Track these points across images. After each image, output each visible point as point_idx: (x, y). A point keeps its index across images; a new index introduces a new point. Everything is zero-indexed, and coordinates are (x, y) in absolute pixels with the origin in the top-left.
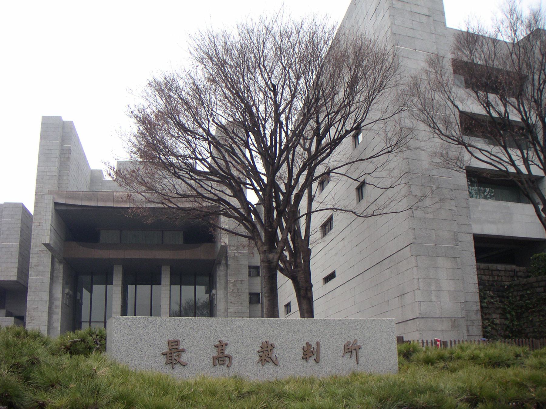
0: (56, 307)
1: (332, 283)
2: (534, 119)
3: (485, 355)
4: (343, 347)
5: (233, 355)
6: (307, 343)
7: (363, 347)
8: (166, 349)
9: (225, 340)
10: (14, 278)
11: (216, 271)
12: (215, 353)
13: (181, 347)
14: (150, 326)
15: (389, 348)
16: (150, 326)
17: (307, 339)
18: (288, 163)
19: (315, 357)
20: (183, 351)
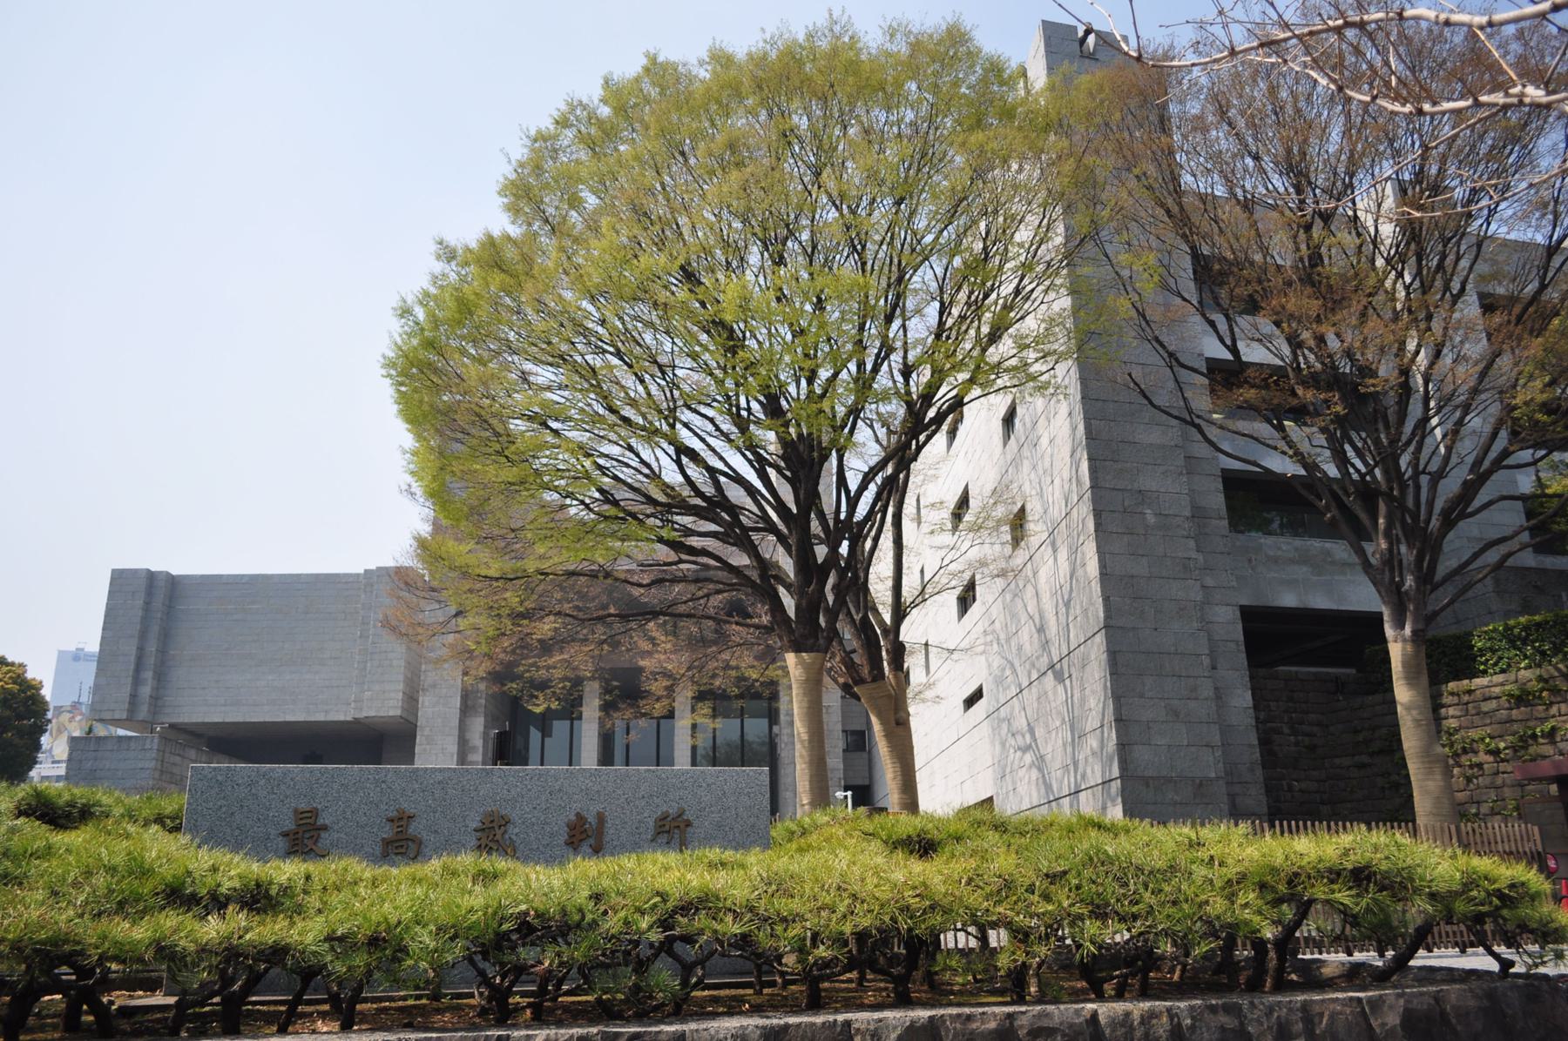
0: (474, 748)
1: (980, 707)
2: (1285, 95)
3: (447, 907)
4: (652, 824)
5: (424, 835)
6: (578, 815)
7: (695, 823)
8: (289, 825)
9: (409, 807)
10: (398, 712)
11: (106, 658)
12: (388, 832)
13: (320, 822)
14: (262, 782)
15: (753, 826)
16: (262, 782)
17: (576, 807)
18: (848, 492)
19: (592, 841)
20: (325, 828)
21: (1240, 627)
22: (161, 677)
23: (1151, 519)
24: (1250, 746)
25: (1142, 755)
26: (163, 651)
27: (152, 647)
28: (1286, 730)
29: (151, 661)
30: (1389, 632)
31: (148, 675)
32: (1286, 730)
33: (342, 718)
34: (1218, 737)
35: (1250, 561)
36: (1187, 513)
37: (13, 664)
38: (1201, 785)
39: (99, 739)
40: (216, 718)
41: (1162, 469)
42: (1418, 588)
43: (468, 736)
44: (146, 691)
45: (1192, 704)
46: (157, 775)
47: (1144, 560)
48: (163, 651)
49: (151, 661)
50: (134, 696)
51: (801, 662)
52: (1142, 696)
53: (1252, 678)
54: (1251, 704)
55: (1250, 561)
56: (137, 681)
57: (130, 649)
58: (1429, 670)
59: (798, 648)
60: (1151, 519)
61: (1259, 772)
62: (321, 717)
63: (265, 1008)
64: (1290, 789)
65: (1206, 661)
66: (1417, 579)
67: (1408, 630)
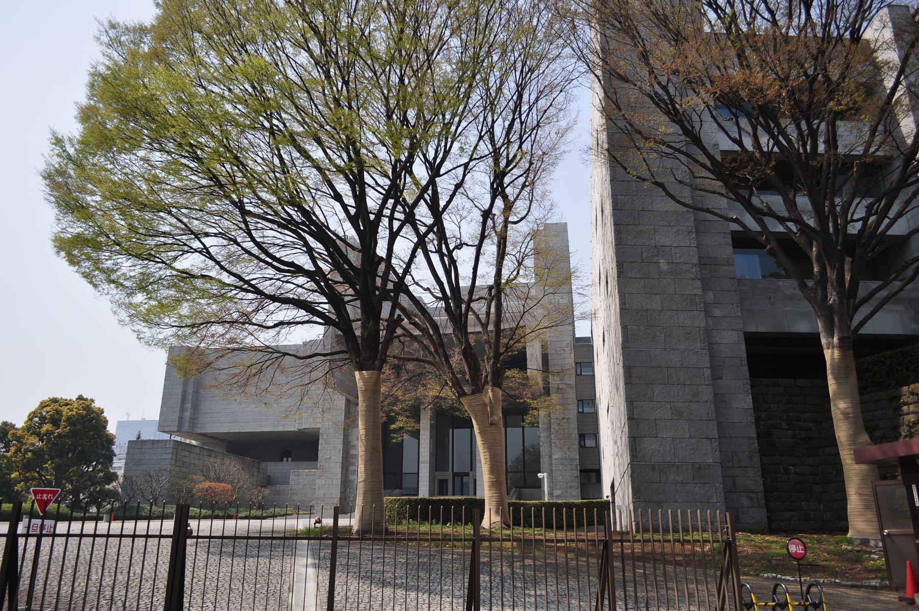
21: (743, 347)
22: (196, 407)
23: (664, 266)
24: (749, 438)
25: (650, 445)
26: (197, 392)
27: (190, 390)
28: (784, 426)
29: (190, 398)
30: (824, 341)
31: (188, 406)
32: (784, 426)
33: (292, 429)
34: (716, 431)
35: (770, 298)
36: (695, 260)
37: (86, 400)
38: (699, 468)
39: (143, 441)
40: (225, 430)
41: (674, 229)
42: (841, 302)
43: (350, 439)
44: (187, 415)
45: (694, 406)
46: (173, 462)
47: (658, 298)
48: (197, 392)
49: (190, 398)
50: (181, 418)
51: (362, 377)
52: (651, 400)
53: (753, 386)
54: (751, 406)
55: (770, 298)
56: (182, 409)
57: (179, 391)
58: (858, 370)
59: (361, 369)
60: (664, 266)
61: (757, 459)
62: (281, 429)
63: (788, 578)
64: (787, 472)
65: (707, 372)
66: (840, 294)
67: (836, 340)
